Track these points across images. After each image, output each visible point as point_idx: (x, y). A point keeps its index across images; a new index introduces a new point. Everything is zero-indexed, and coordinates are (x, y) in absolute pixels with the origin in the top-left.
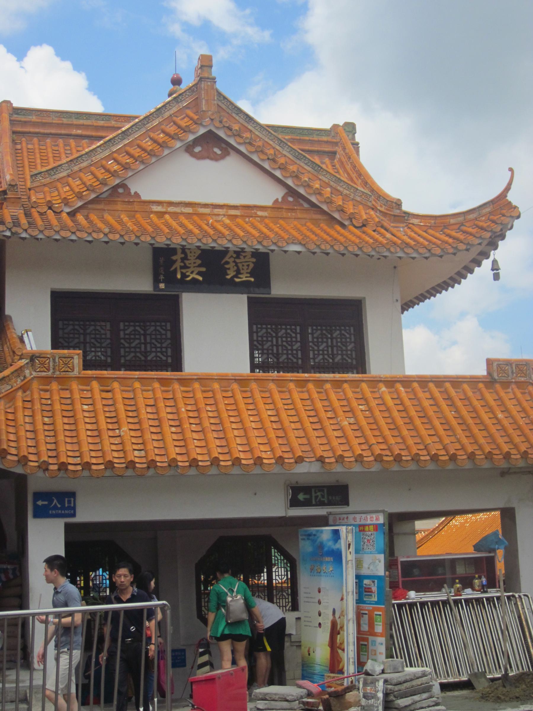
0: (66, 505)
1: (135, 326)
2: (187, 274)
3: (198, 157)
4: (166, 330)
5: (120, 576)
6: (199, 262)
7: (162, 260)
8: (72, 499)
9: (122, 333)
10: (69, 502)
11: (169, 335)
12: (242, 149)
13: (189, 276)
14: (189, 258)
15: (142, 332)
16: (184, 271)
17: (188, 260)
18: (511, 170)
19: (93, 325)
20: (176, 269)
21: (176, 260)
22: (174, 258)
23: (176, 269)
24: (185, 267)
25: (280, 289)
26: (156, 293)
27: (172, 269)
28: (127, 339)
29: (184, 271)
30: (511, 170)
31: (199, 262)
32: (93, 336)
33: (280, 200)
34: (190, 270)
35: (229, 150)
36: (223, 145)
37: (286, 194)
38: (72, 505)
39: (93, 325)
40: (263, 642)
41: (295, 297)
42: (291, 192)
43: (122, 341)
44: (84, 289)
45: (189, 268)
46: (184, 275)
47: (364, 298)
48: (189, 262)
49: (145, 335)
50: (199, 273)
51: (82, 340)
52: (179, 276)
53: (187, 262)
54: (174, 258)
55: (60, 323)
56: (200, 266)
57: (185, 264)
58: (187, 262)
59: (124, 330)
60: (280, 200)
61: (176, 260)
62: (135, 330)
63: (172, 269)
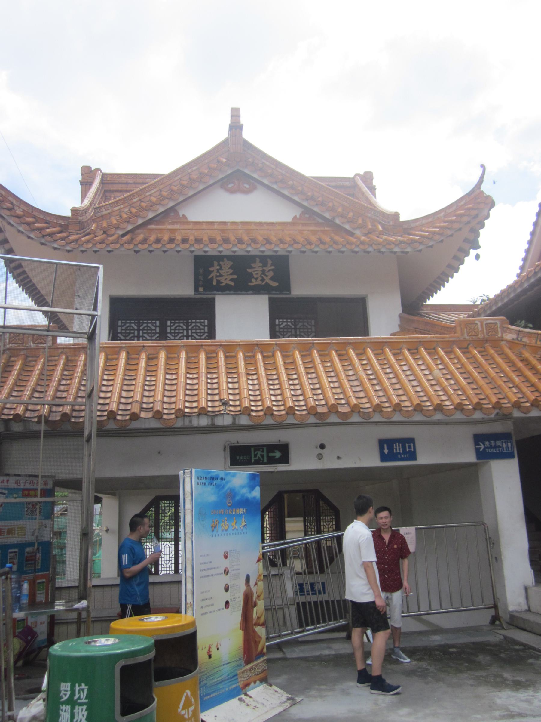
0: (407, 450)
1: (287, 322)
2: (222, 281)
3: (232, 191)
4: (156, 326)
5: (382, 518)
6: (231, 271)
7: (201, 271)
8: (412, 445)
9: (119, 329)
10: (410, 447)
11: (206, 329)
12: (266, 181)
13: (222, 283)
14: (223, 268)
15: (185, 327)
16: (219, 279)
17: (222, 270)
18: (482, 166)
19: (145, 323)
20: (213, 277)
21: (213, 271)
22: (211, 269)
23: (213, 277)
24: (221, 276)
25: (299, 289)
26: (198, 296)
27: (210, 277)
28: (124, 333)
29: (219, 279)
30: (482, 166)
31: (231, 271)
32: (202, 331)
33: (298, 216)
34: (224, 278)
35: (256, 184)
36: (252, 181)
37: (303, 212)
38: (412, 450)
39: (145, 323)
40: (43, 677)
41: (316, 297)
42: (307, 211)
43: (169, 335)
44: (145, 295)
45: (223, 276)
46: (219, 282)
47: (110, 295)
48: (223, 271)
49: (187, 330)
50: (232, 280)
51: (185, 334)
52: (215, 283)
53: (221, 272)
54: (211, 269)
55: (277, 321)
56: (231, 274)
57: (220, 273)
58: (221, 272)
59: (279, 325)
60: (298, 216)
61: (213, 271)
62: (304, 325)
63: (210, 277)
